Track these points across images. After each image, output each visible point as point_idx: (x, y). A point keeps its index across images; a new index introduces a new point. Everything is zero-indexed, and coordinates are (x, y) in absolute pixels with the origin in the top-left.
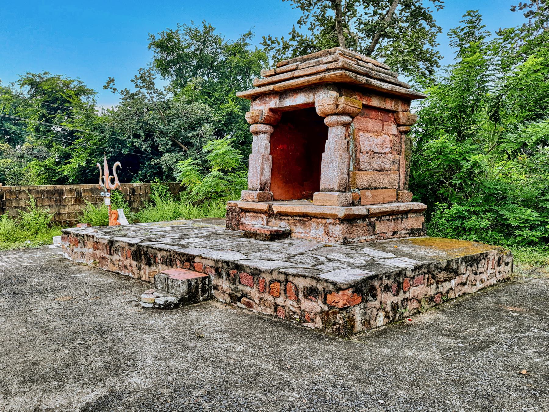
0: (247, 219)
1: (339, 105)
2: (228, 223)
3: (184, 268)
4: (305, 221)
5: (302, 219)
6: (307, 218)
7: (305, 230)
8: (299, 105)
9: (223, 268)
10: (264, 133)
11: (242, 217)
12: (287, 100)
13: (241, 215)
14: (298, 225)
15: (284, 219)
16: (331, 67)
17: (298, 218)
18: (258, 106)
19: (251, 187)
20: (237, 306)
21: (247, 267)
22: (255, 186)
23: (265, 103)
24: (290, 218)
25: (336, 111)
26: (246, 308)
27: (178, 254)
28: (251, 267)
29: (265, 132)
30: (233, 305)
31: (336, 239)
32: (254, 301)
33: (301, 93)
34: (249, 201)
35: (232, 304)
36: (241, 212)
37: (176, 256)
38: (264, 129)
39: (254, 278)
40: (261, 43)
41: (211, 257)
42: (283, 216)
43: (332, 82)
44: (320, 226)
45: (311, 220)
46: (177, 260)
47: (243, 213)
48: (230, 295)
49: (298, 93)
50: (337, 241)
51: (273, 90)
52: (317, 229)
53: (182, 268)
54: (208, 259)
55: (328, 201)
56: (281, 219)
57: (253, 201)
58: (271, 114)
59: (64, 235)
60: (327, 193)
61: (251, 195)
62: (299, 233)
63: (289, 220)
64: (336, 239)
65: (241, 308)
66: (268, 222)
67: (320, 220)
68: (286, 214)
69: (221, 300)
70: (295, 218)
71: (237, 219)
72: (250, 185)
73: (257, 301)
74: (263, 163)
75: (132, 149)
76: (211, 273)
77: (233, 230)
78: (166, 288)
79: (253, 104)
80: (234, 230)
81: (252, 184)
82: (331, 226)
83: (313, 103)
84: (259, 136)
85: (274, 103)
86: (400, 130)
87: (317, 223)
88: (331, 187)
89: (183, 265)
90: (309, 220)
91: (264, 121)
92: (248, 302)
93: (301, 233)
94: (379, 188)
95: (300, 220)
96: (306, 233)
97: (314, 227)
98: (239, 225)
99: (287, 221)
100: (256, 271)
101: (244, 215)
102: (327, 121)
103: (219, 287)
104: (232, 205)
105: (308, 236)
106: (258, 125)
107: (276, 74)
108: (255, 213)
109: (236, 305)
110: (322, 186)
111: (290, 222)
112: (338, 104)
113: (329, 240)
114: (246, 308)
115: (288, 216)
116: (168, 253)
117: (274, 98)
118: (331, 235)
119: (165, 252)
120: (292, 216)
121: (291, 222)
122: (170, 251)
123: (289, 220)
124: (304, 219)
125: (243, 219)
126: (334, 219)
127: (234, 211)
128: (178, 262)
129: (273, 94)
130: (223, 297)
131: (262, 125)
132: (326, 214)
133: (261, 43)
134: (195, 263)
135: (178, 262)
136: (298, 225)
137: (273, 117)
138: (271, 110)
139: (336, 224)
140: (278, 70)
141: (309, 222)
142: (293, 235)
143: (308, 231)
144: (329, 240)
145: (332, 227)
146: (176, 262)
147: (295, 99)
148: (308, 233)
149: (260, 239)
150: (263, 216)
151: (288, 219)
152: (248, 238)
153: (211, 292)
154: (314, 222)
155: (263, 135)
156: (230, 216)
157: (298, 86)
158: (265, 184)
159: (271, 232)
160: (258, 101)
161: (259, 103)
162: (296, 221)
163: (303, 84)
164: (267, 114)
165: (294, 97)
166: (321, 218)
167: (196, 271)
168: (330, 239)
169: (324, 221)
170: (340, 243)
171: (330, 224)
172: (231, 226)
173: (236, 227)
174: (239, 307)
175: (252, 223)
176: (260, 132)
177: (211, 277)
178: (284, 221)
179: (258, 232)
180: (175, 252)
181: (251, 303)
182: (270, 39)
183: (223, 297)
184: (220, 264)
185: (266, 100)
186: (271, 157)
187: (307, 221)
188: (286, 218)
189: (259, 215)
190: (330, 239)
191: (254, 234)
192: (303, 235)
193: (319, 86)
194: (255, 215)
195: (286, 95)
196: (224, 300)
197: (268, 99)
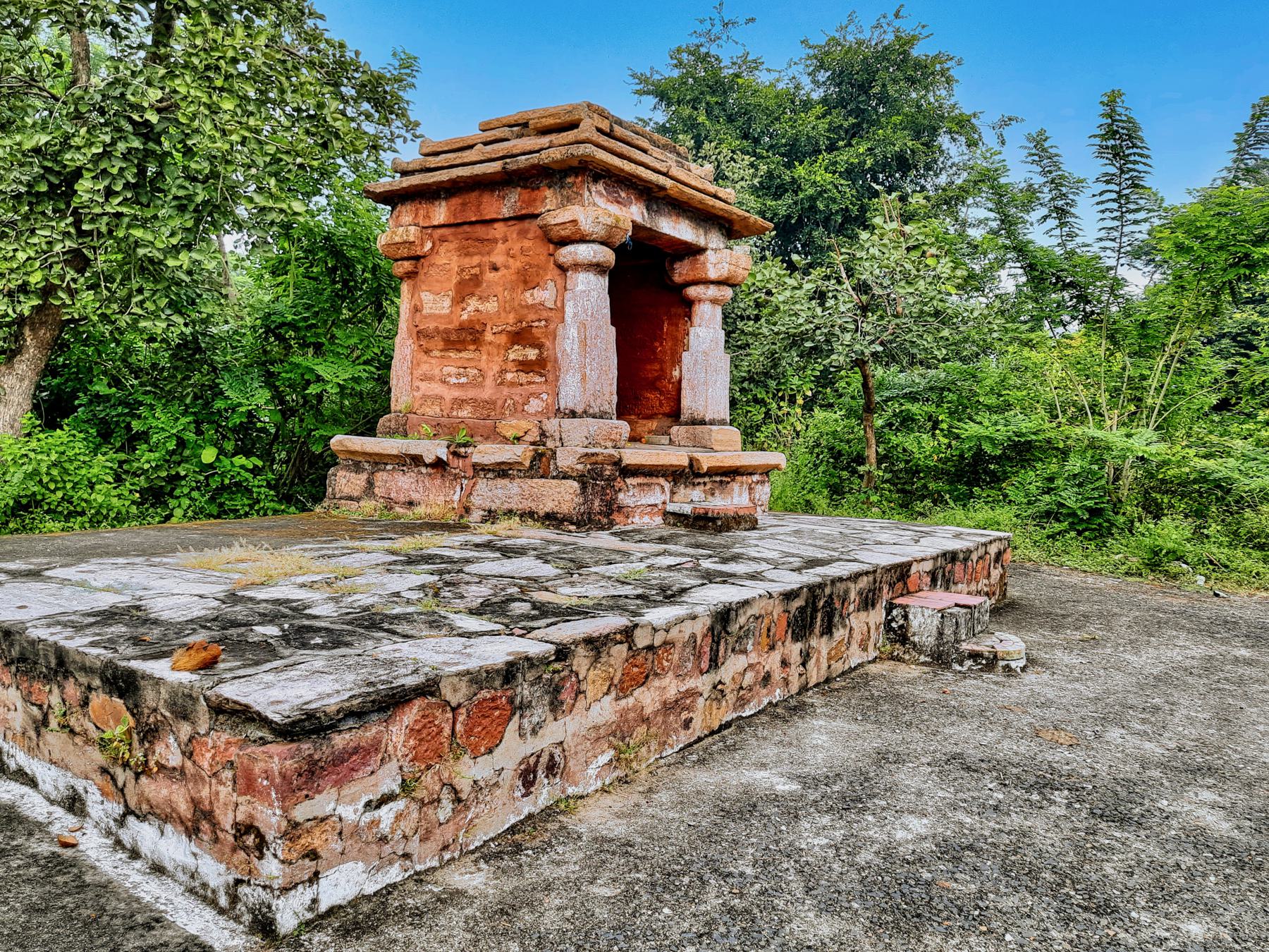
17: (718, 479)
22: (606, 407)
24: (707, 479)
56: (694, 485)
59: (964, 637)
75: (347, 78)
81: (599, 401)
85: (636, 212)
94: (585, 413)
116: (871, 578)
121: (708, 487)
125: (621, 496)
127: (600, 475)
132: (750, 466)
150: (662, 481)
156: (590, 490)
157: (678, 215)
172: (590, 520)
173: (605, 520)
175: (643, 502)
179: (741, 513)
189: (654, 480)
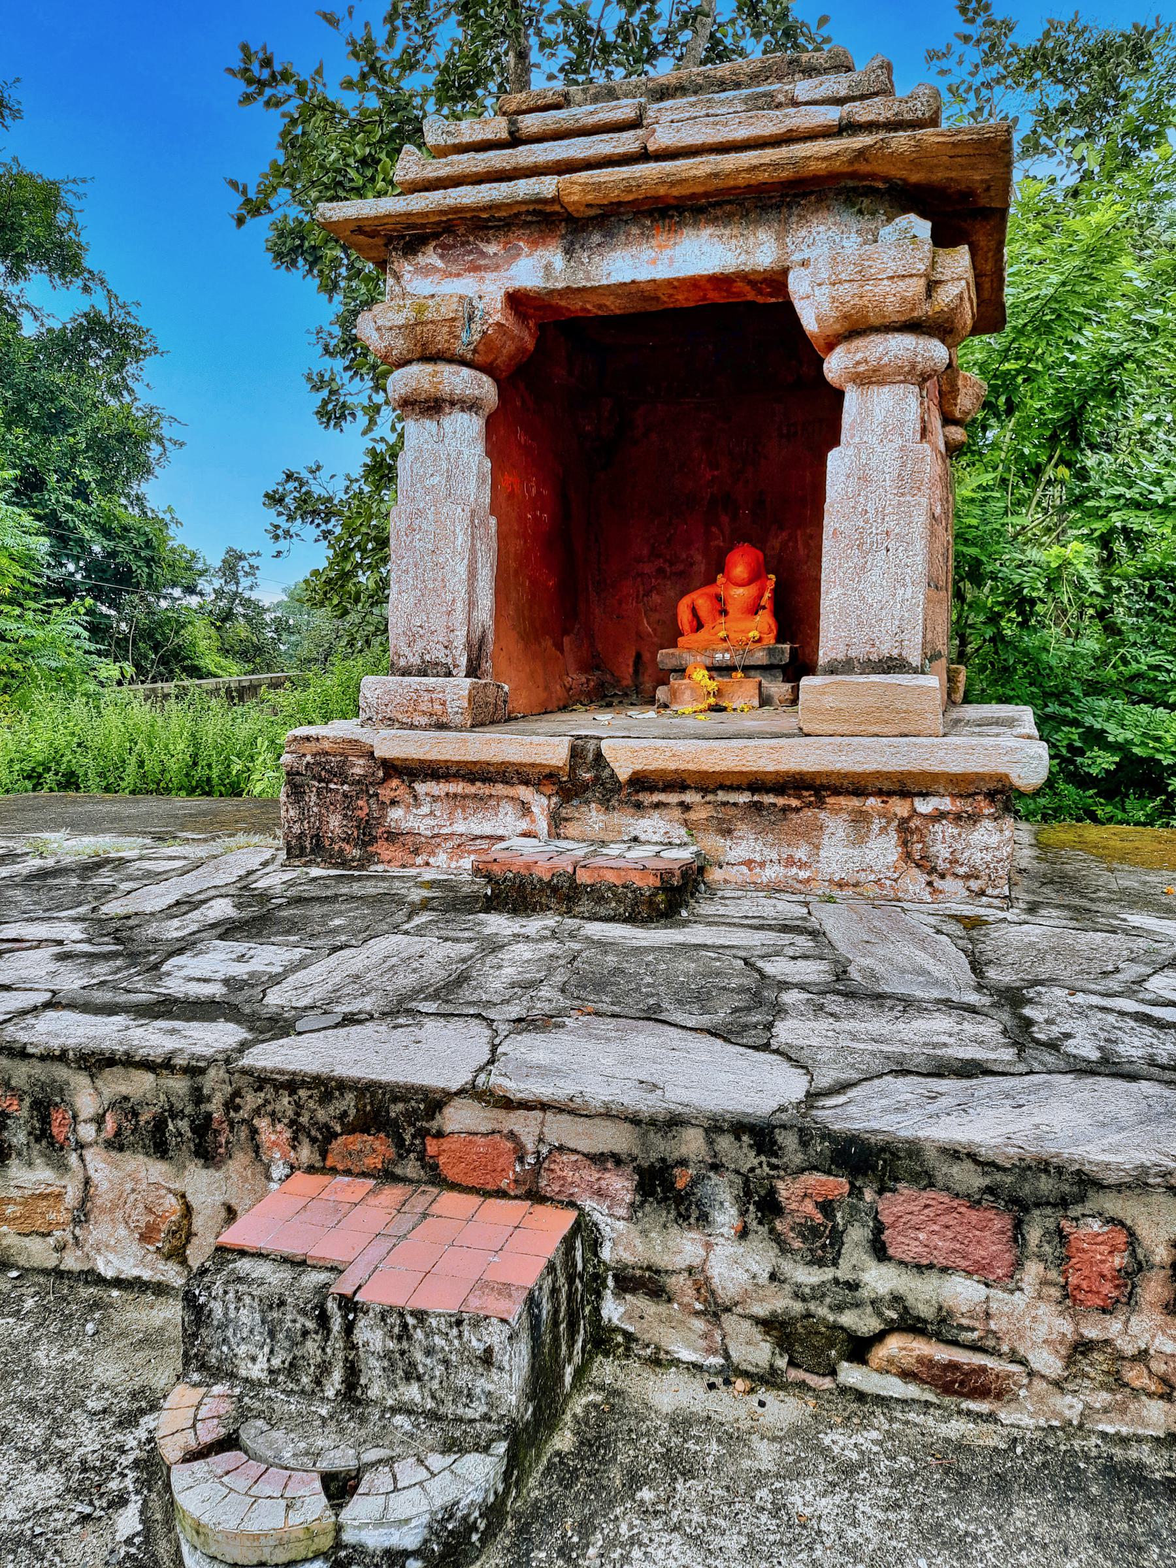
0: (425, 810)
1: (939, 282)
2: (301, 836)
3: (333, 1171)
4: (785, 809)
5: (769, 799)
6: (799, 797)
7: (789, 851)
8: (693, 283)
9: (715, 1167)
10: (470, 408)
11: (394, 803)
12: (617, 254)
13: (385, 793)
14: (742, 829)
15: (658, 805)
16: (872, 117)
17: (743, 798)
18: (437, 277)
19: (415, 661)
20: (844, 1390)
21: (953, 1154)
23: (476, 268)
25: (925, 310)
26: (931, 1398)
27: (278, 1086)
28: (984, 1153)
29: (470, 405)
30: (802, 1385)
31: (975, 885)
32: (1023, 1362)
33: (696, 224)
34: (412, 727)
35: (794, 1374)
36: (387, 778)
37: (251, 1100)
38: (472, 392)
39: (1018, 1225)
40: (230, 71)
41: (599, 1093)
42: (652, 789)
43: (886, 179)
44: (875, 827)
45: (820, 803)
46: (262, 1123)
47: (395, 783)
48: (769, 1324)
49: (681, 224)
50: (982, 893)
51: (556, 200)
52: (859, 840)
53: (311, 1169)
54: (572, 1112)
55: (885, 716)
56: (638, 806)
57: (442, 726)
58: (510, 322)
60: (862, 679)
61: (427, 697)
62: (749, 863)
63: (685, 807)
64: (975, 885)
65: (882, 1401)
66: (557, 821)
67: (872, 801)
68: (676, 782)
69: (686, 1355)
70: (722, 796)
71: (362, 814)
72: (405, 650)
73: (1048, 1362)
74: (473, 550)
76: (600, 1194)
77: (336, 866)
78: (325, 1368)
79: (406, 268)
80: (344, 864)
82: (945, 829)
83: (776, 281)
84: (446, 421)
86: (951, 437)
87: (860, 819)
88: (887, 648)
89: (324, 1154)
90: (809, 805)
91: (475, 351)
92: (953, 1366)
93: (762, 865)
95: (757, 807)
96: (790, 862)
97: (841, 833)
98: (374, 840)
99: (677, 813)
100: (1046, 1185)
101: (402, 792)
102: (835, 366)
103: (676, 1283)
104: (326, 745)
105: (803, 875)
106: (446, 369)
107: (515, 140)
108: (472, 781)
109: (827, 1383)
110: (824, 656)
111: (692, 816)
112: (938, 277)
113: (935, 891)
114: (931, 1398)
115: (683, 787)
116: (179, 1085)
117: (534, 244)
118: (942, 866)
119: (149, 1078)
120: (704, 790)
122: (193, 1071)
123: (685, 807)
124: (781, 801)
125: (395, 813)
126: (953, 796)
128: (271, 1135)
129: (527, 224)
130: (705, 1336)
131: (465, 372)
133: (230, 71)
134: (440, 1134)
135: (271, 1135)
136: (742, 829)
137: (513, 339)
138: (516, 301)
139: (974, 818)
140: (531, 123)
141: (808, 813)
142: (715, 875)
143: (801, 854)
144: (935, 891)
145: (952, 830)
146: (254, 1131)
147: (668, 252)
148: (802, 865)
149: (602, 911)
150: (524, 793)
151: (681, 804)
152: (515, 911)
153: (597, 1310)
154: (836, 811)
155: (466, 416)
157: (717, 183)
158: (482, 641)
159: (664, 875)
160: (430, 257)
161: (439, 263)
162: (732, 811)
163: (741, 181)
164: (498, 317)
165: (654, 242)
166: (880, 793)
167: (454, 1186)
168: (939, 883)
169: (900, 807)
170: (996, 902)
171: (939, 816)
173: (356, 853)
174: (861, 1397)
176: (453, 404)
177: (597, 1216)
178: (656, 814)
179: (583, 877)
180: (244, 1072)
181: (983, 1370)
182: (267, 62)
183: (705, 1336)
184: (692, 1143)
185: (483, 254)
186: (493, 521)
187: (797, 810)
188: (673, 798)
189: (500, 789)
190: (939, 883)
191: (555, 889)
192: (770, 873)
193: (805, 195)
194: (471, 789)
195: (609, 234)
196: (710, 1351)
197: (491, 249)
